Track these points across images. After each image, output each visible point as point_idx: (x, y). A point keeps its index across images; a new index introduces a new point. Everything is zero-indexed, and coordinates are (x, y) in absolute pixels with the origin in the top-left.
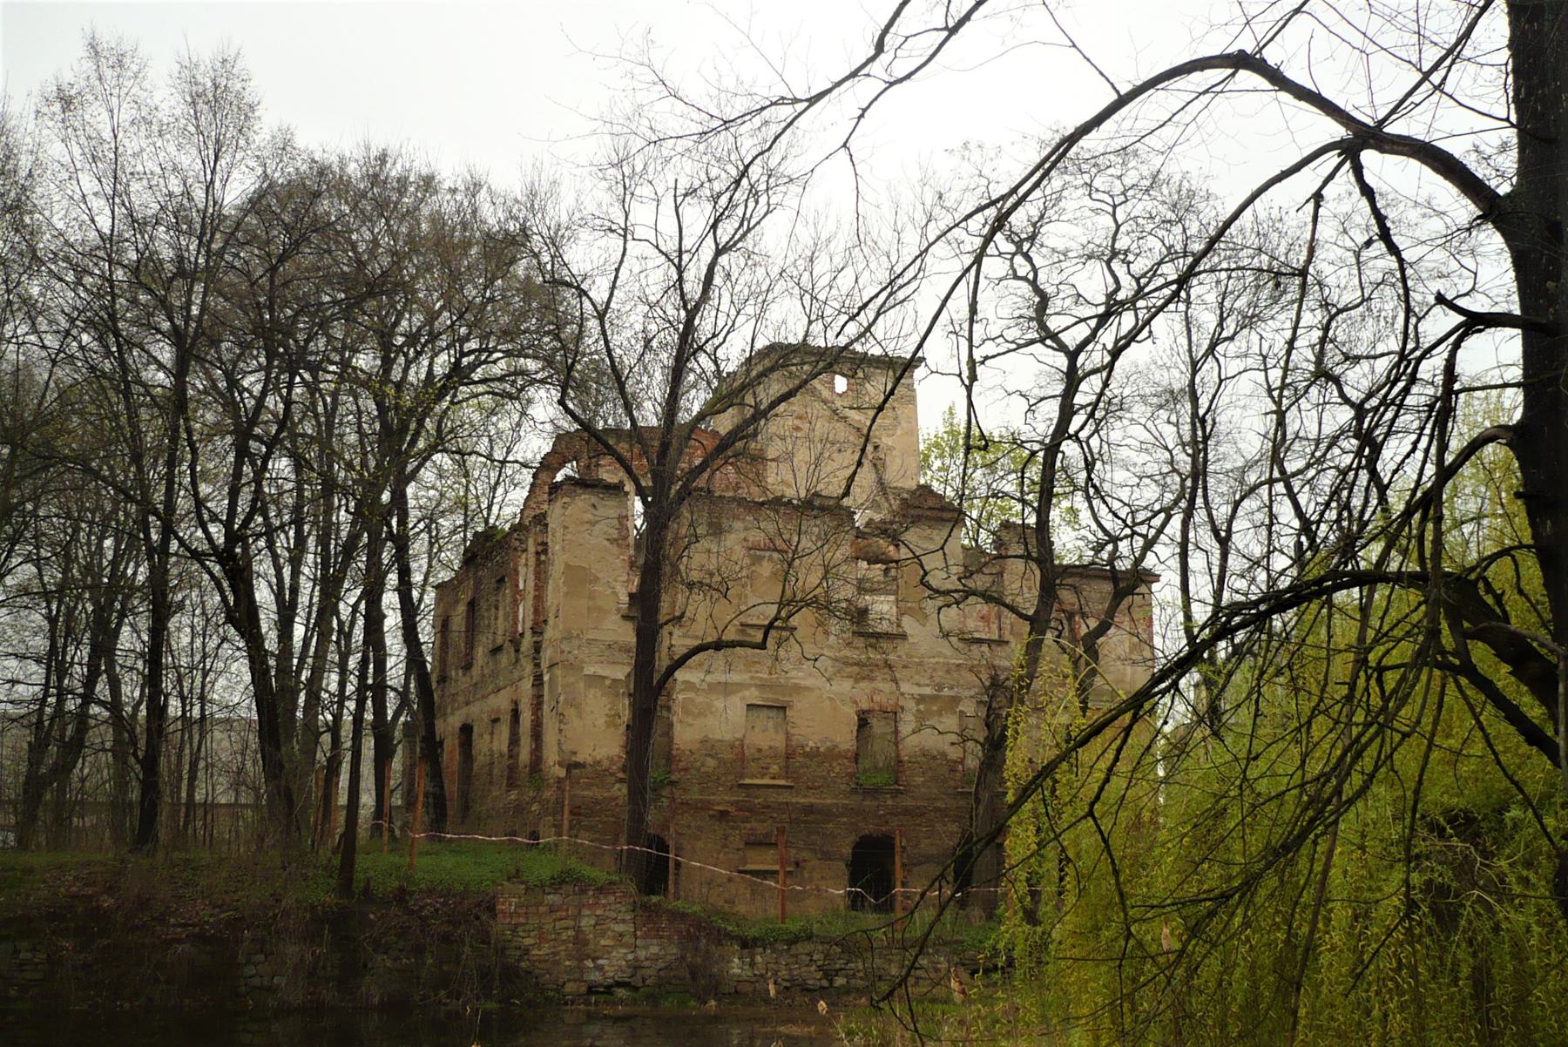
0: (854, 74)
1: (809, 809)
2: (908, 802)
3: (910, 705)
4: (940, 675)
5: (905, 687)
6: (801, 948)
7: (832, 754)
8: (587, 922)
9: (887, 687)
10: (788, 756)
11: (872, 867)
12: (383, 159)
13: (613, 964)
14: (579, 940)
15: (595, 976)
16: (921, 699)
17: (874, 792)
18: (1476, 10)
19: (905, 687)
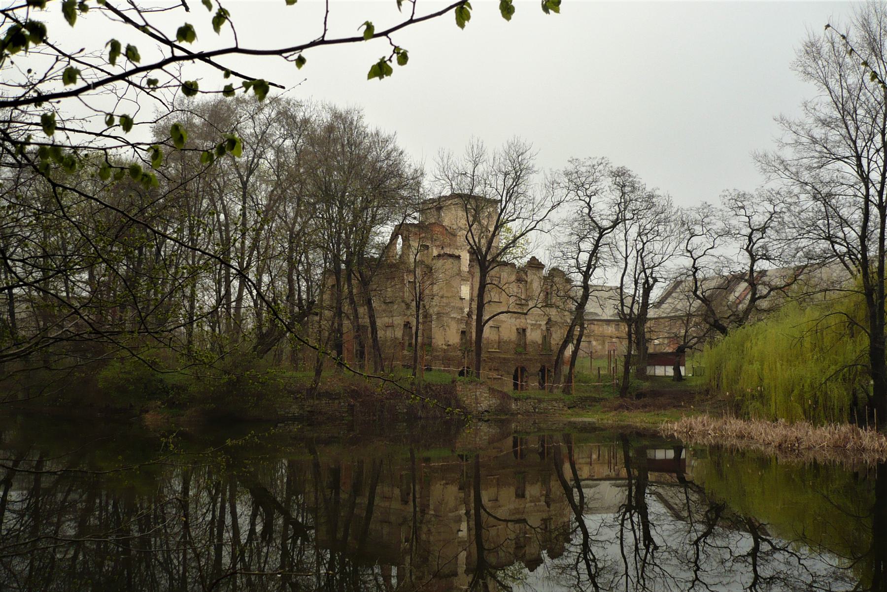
0: (279, 52)
1: (504, 359)
2: (528, 357)
3: (529, 327)
4: (537, 318)
5: (528, 321)
6: (529, 401)
7: (510, 341)
8: (478, 393)
9: (523, 321)
10: (499, 342)
11: (519, 374)
12: (26, 51)
13: (484, 405)
14: (476, 399)
15: (480, 409)
16: (532, 325)
17: (520, 354)
18: (285, 55)
19: (528, 321)
